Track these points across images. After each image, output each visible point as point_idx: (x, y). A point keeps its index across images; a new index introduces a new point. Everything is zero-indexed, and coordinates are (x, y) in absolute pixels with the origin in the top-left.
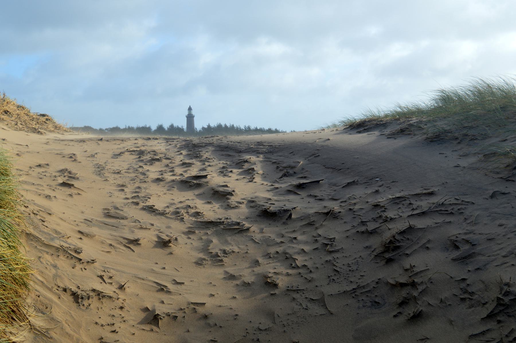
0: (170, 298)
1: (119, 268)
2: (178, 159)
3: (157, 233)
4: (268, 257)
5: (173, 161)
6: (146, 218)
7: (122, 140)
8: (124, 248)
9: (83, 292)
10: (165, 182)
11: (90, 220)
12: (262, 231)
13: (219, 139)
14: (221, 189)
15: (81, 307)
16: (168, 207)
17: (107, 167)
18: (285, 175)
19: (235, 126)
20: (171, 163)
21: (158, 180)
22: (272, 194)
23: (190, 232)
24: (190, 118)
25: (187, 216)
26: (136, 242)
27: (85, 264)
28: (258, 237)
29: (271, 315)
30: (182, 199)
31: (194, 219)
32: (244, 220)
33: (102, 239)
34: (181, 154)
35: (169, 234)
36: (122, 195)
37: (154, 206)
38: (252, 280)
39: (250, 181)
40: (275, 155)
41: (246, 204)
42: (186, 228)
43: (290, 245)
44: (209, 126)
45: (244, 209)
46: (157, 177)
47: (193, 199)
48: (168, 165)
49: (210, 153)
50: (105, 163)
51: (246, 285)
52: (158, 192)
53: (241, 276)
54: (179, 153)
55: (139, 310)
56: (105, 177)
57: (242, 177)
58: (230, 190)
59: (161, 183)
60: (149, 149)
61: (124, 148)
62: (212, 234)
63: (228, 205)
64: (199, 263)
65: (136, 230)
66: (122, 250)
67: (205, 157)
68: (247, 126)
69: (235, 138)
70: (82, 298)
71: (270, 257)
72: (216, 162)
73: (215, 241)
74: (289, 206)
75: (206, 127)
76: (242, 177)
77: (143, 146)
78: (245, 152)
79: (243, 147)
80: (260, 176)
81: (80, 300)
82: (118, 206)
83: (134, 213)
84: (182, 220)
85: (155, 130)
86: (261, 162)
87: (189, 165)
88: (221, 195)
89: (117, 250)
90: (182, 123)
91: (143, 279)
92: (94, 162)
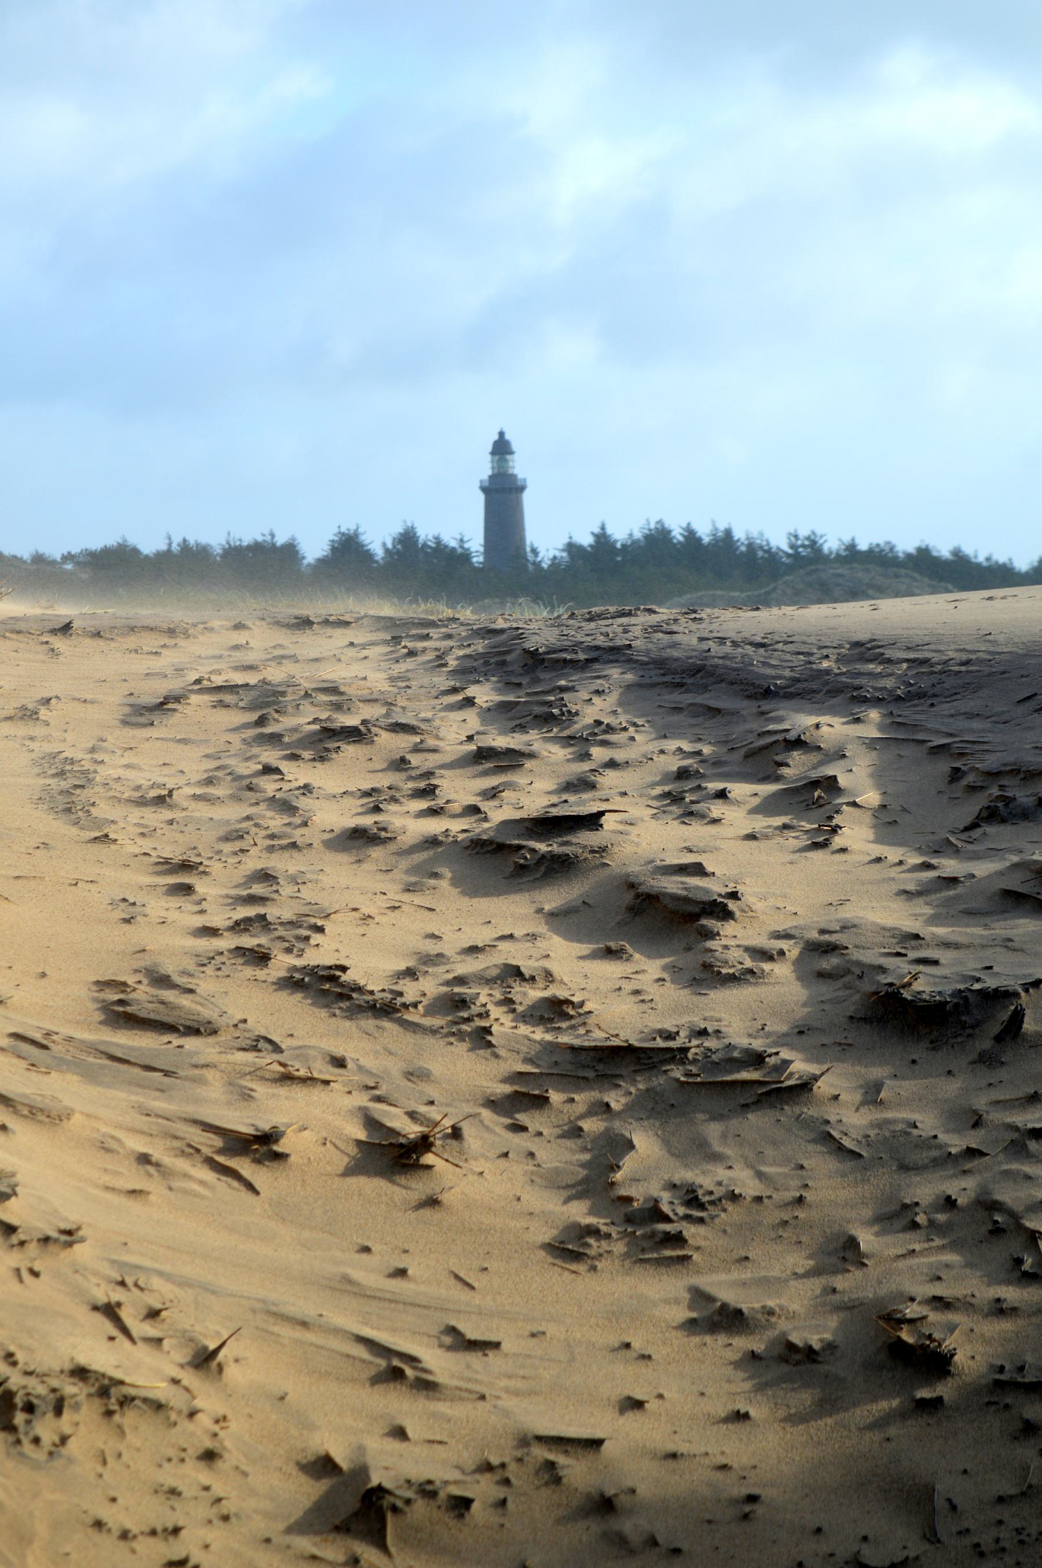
0: (434, 1415)
1: (188, 1270)
2: (455, 731)
3: (362, 1100)
4: (904, 1221)
5: (431, 742)
6: (309, 1029)
7: (171, 632)
8: (208, 1175)
9: (32, 1382)
10: (392, 847)
11: (38, 1036)
12: (872, 1094)
13: (657, 628)
14: (672, 885)
15: (27, 1447)
16: (410, 973)
17: (104, 773)
18: (991, 815)
19: (739, 534)
20: (417, 749)
21: (359, 839)
22: (929, 911)
23: (520, 1101)
24: (503, 495)
25: (507, 1020)
26: (263, 1146)
27: (32, 1248)
28: (853, 1121)
29: (918, 1500)
30: (482, 936)
31: (540, 1034)
32: (783, 1040)
33: (104, 1129)
34: (469, 702)
35: (423, 1109)
36: (184, 915)
37: (344, 969)
38: (828, 1336)
39: (816, 846)
40: (945, 708)
41: (798, 962)
42: (505, 1080)
43: (1015, 1166)
44: (602, 539)
45: (784, 987)
46: (352, 823)
47: (533, 937)
48: (403, 760)
49: (612, 699)
50: (93, 750)
51: (794, 1360)
52: (357, 901)
53: (771, 1313)
54: (459, 697)
55: (294, 1471)
56: (98, 823)
57: (779, 821)
58: (715, 887)
59: (376, 853)
60: (306, 676)
61: (179, 670)
62: (629, 1108)
63: (707, 967)
64: (570, 1248)
65: (261, 1090)
66: (202, 1183)
67: (589, 721)
68: (803, 533)
69: (735, 623)
70: (30, 1408)
71: (915, 1226)
72: (644, 742)
73: (645, 1143)
74: (1007, 973)
75: (586, 540)
76: (779, 821)
77: (280, 659)
78: (789, 696)
79: (779, 669)
80: (867, 818)
81: (20, 1418)
82: (169, 968)
83: (245, 1000)
84: (482, 1038)
85: (322, 562)
86: (872, 744)
87: (509, 760)
88: (673, 918)
89: (176, 1184)
90: (464, 526)
91: (304, 1324)
92: (33, 745)
